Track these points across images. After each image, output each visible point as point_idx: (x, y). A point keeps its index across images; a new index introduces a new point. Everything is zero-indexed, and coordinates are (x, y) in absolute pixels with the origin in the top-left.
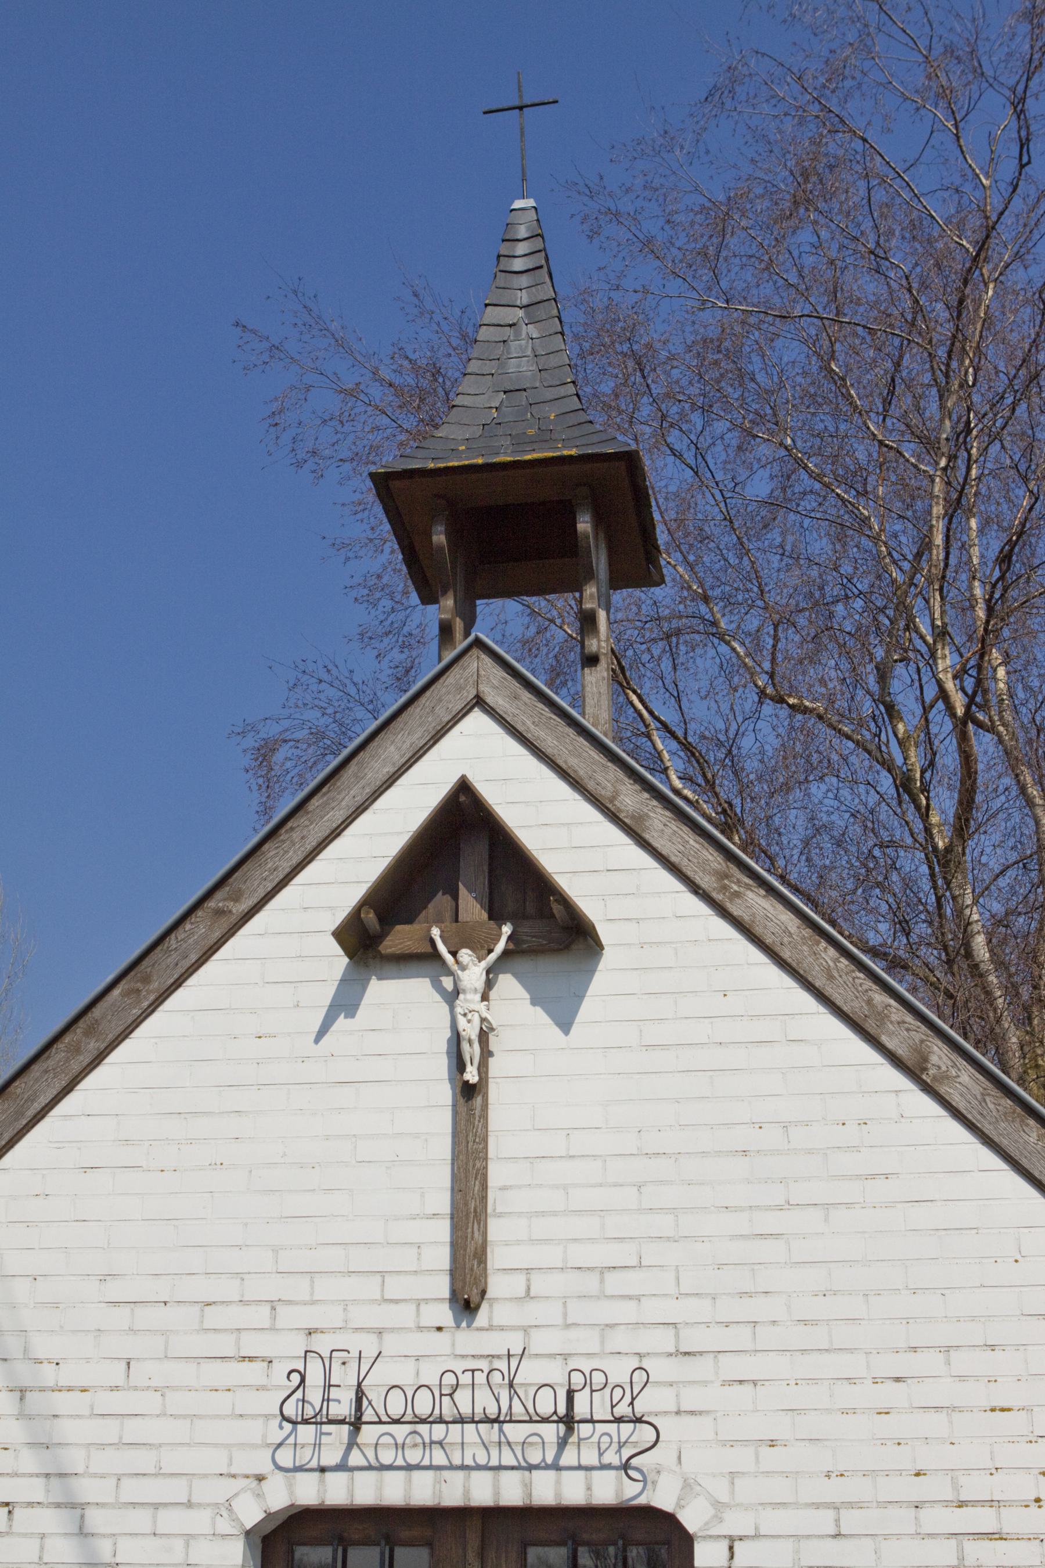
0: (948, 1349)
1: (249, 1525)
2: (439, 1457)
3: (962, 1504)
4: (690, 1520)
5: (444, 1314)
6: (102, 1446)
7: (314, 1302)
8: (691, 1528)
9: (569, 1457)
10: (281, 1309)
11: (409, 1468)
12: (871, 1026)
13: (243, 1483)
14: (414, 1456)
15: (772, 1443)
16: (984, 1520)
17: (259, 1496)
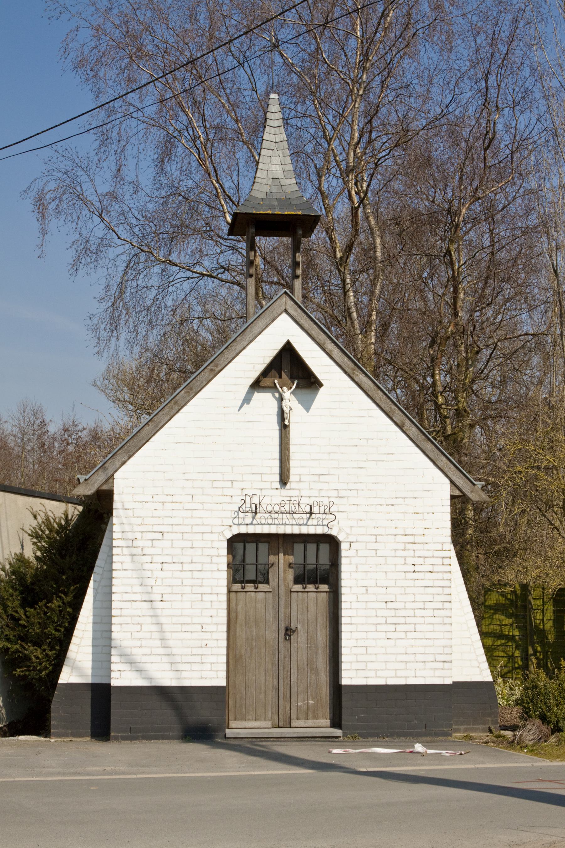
1: (228, 538)
3: (406, 535)
4: (341, 538)
5: (278, 485)
6: (187, 517)
7: (243, 481)
9: (255, 522)
10: (234, 483)
12: (390, 414)
14: (270, 521)
15: (361, 520)
16: (411, 539)
17: (231, 530)
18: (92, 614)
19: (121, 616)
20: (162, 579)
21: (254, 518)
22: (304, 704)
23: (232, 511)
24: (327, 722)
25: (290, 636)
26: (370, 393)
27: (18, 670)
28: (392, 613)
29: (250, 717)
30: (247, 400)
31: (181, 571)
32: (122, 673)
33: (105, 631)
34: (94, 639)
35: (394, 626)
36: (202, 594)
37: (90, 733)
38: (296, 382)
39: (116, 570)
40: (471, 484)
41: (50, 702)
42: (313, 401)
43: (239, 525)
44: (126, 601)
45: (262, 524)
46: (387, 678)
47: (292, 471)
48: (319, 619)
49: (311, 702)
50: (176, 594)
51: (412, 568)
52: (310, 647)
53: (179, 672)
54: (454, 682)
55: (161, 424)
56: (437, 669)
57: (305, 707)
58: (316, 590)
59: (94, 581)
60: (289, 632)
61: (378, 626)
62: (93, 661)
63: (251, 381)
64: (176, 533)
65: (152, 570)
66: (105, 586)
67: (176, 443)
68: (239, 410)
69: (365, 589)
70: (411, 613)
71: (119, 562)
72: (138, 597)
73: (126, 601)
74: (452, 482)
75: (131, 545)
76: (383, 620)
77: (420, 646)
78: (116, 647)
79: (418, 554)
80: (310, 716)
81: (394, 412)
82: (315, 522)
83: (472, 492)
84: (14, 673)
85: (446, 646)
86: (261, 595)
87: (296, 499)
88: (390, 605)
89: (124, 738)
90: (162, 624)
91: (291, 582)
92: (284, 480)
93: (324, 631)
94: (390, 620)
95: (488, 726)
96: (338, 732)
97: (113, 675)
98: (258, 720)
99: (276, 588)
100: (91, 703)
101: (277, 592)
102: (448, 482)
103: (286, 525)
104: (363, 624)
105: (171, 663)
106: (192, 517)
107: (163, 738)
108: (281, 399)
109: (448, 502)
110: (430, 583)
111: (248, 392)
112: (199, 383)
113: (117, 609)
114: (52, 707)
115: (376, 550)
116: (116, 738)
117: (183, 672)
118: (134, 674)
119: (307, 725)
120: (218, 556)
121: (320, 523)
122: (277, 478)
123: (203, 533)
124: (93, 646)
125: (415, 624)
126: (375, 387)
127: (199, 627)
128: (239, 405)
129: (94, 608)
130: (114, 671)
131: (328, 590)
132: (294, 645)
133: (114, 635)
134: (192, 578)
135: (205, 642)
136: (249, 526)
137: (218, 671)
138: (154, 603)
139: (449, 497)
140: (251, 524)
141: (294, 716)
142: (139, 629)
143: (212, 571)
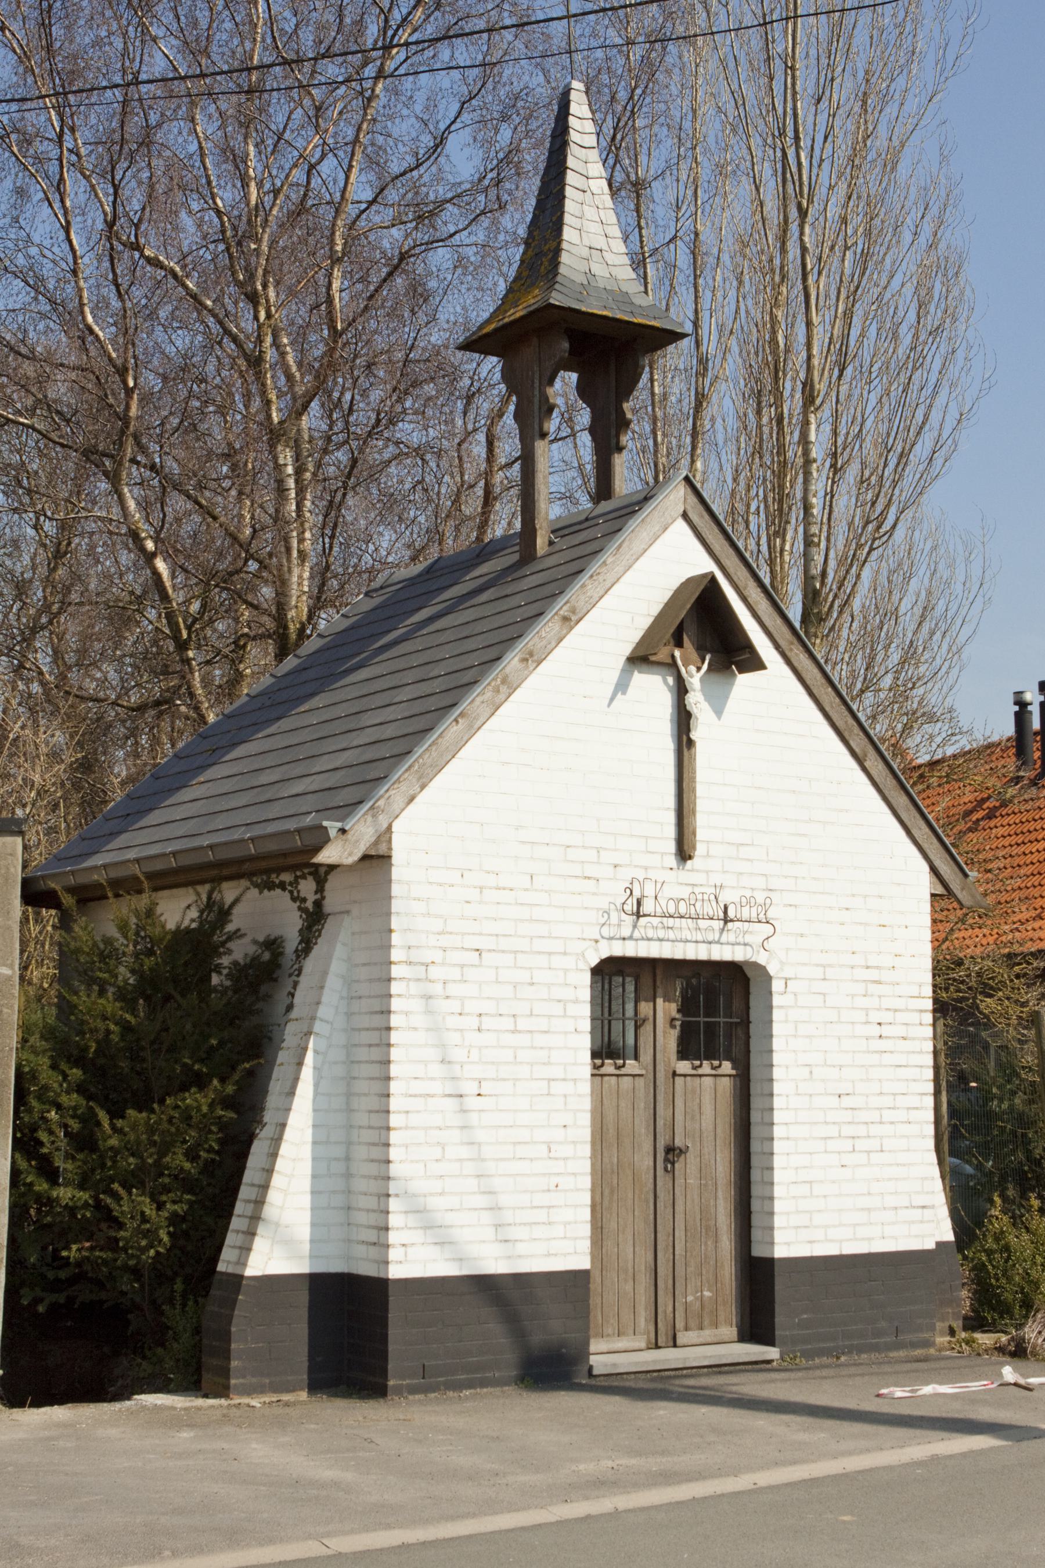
0: (865, 897)
1: (593, 965)
2: (672, 936)
3: (868, 967)
4: (772, 970)
5: (672, 861)
6: (522, 921)
7: (616, 850)
8: (772, 973)
9: (636, 934)
10: (602, 852)
11: (661, 940)
12: (846, 735)
13: (589, 943)
14: (661, 933)
15: (802, 935)
16: (874, 974)
17: (597, 950)
18: (310, 1123)
19: (407, 1128)
20: (480, 1048)
21: (635, 926)
22: (696, 1298)
23: (598, 909)
24: (731, 1332)
25: (673, 1164)
26: (815, 691)
27: (74, 1247)
28: (848, 1116)
29: (610, 1331)
30: (622, 686)
31: (513, 1032)
32: (410, 1250)
33: (335, 1159)
34: (314, 1176)
35: (850, 1142)
36: (549, 1080)
37: (306, 1382)
38: (708, 657)
39: (397, 1029)
40: (960, 875)
41: (229, 1319)
42: (727, 698)
43: (611, 938)
44: (415, 1096)
45: (649, 939)
46: (841, 1241)
47: (701, 834)
48: (719, 1131)
49: (707, 1294)
50: (504, 1080)
51: (876, 1030)
52: (706, 1185)
53: (510, 1244)
54: (938, 1244)
55: (479, 723)
56: (913, 1222)
57: (698, 1304)
58: (714, 1072)
59: (316, 1052)
60: (673, 1153)
61: (829, 1142)
62: (313, 1225)
63: (627, 650)
64: (503, 952)
65: (461, 1030)
66: (335, 1063)
67: (504, 763)
68: (609, 705)
69: (807, 1069)
70: (875, 1116)
71: (402, 1012)
72: (436, 1087)
73: (415, 1096)
74: (934, 870)
75: (423, 976)
76: (833, 1131)
77: (890, 1179)
78: (397, 1195)
79: (887, 1003)
80: (706, 1323)
81: (851, 731)
82: (732, 938)
83: (963, 889)
84: (64, 1254)
85: (926, 1178)
86: (626, 1082)
87: (713, 890)
88: (846, 1101)
89: (413, 1390)
90: (479, 1144)
91: (673, 1056)
92: (684, 852)
93: (726, 1152)
94: (847, 1130)
95: (947, 1324)
96: (772, 1353)
97: (393, 1254)
98: (624, 1334)
99: (651, 1068)
100: (309, 1317)
101: (651, 1076)
102: (926, 867)
103: (687, 941)
104: (805, 1139)
105: (497, 1226)
106: (531, 920)
107: (484, 1383)
108: (681, 690)
109: (927, 907)
110: (902, 1060)
111: (623, 670)
112: (544, 642)
113: (399, 1112)
114: (233, 1329)
115: (824, 995)
116: (399, 1391)
117: (519, 1245)
118: (433, 1252)
119: (701, 1340)
120: (576, 1001)
121: (740, 940)
122: (671, 847)
123: (550, 954)
124: (313, 1193)
125: (881, 1138)
126: (824, 681)
127: (545, 1148)
128: (609, 696)
129: (314, 1110)
130: (394, 1246)
131: (734, 1072)
132: (679, 1181)
133: (394, 1169)
134: (532, 1047)
135: (554, 1180)
136: (627, 942)
137: (576, 1239)
138: (466, 1099)
139: (928, 897)
140: (631, 938)
141: (680, 1324)
142: (439, 1157)
143: (566, 1033)
